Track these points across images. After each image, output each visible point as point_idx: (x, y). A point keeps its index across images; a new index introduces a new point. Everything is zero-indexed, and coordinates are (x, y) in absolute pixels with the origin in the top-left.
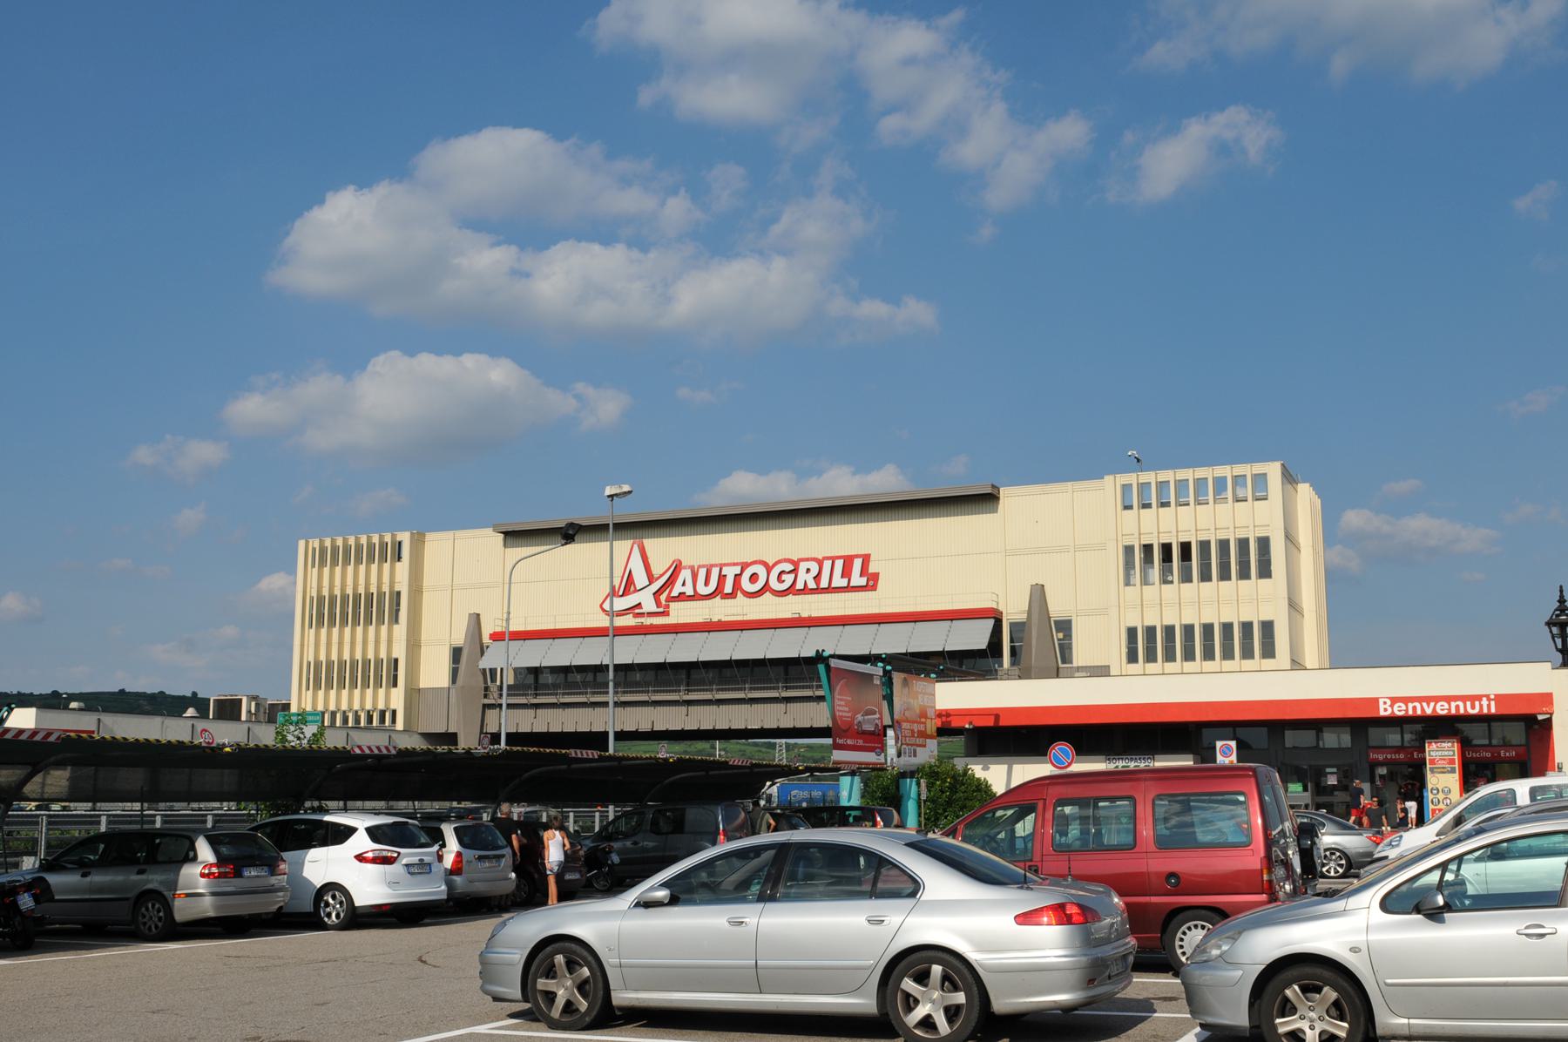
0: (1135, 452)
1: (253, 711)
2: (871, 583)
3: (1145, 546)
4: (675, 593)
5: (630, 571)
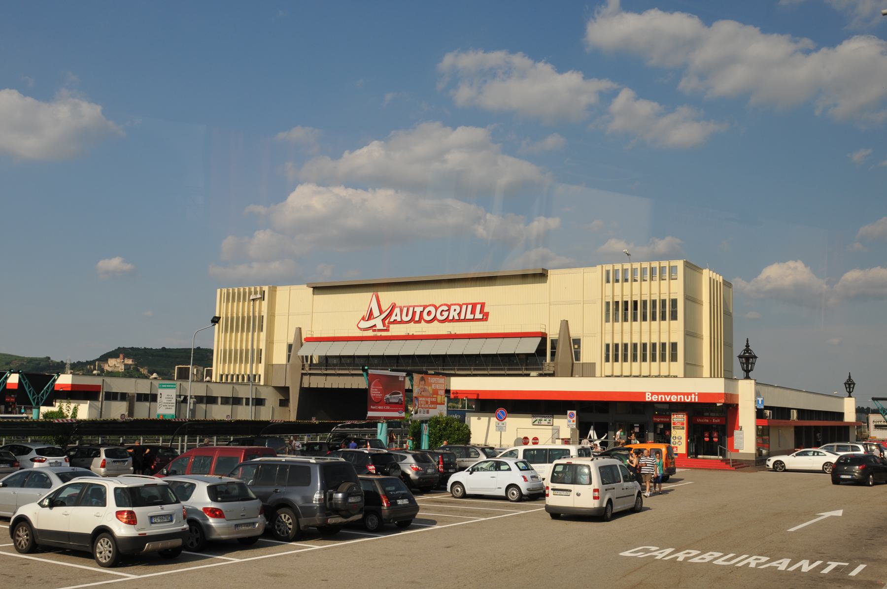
1: (195, 373)
2: (485, 317)
3: (616, 302)
4: (392, 320)
5: (371, 309)
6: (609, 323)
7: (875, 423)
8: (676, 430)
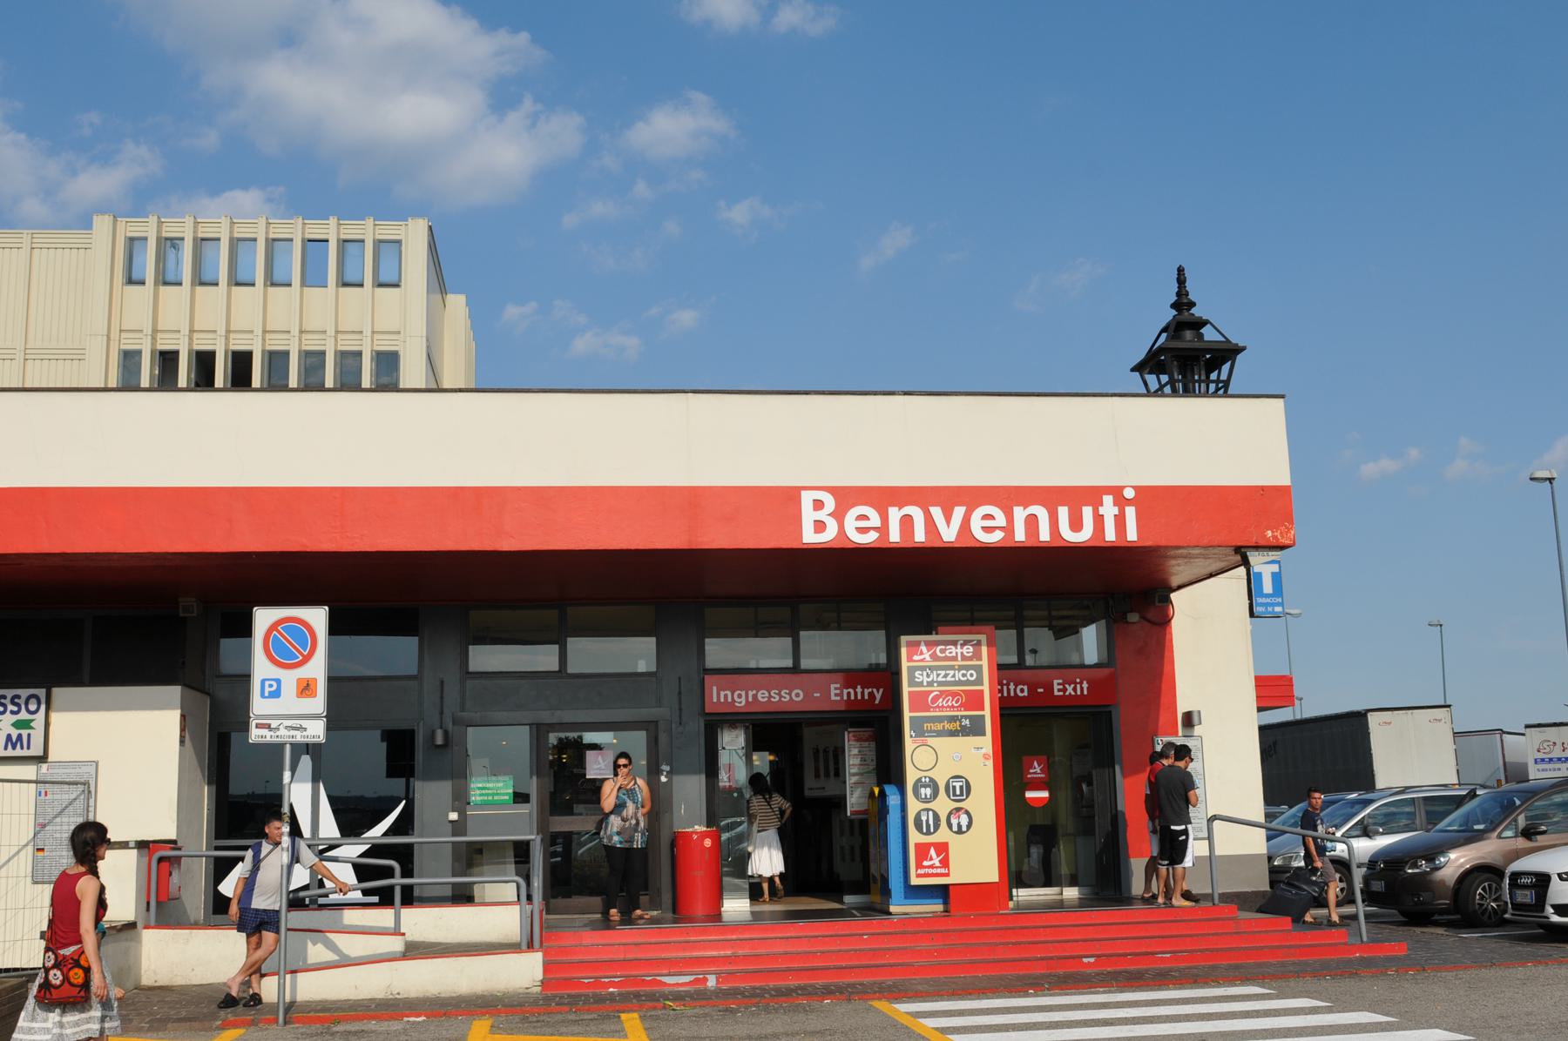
3: (163, 354)
8: (932, 741)
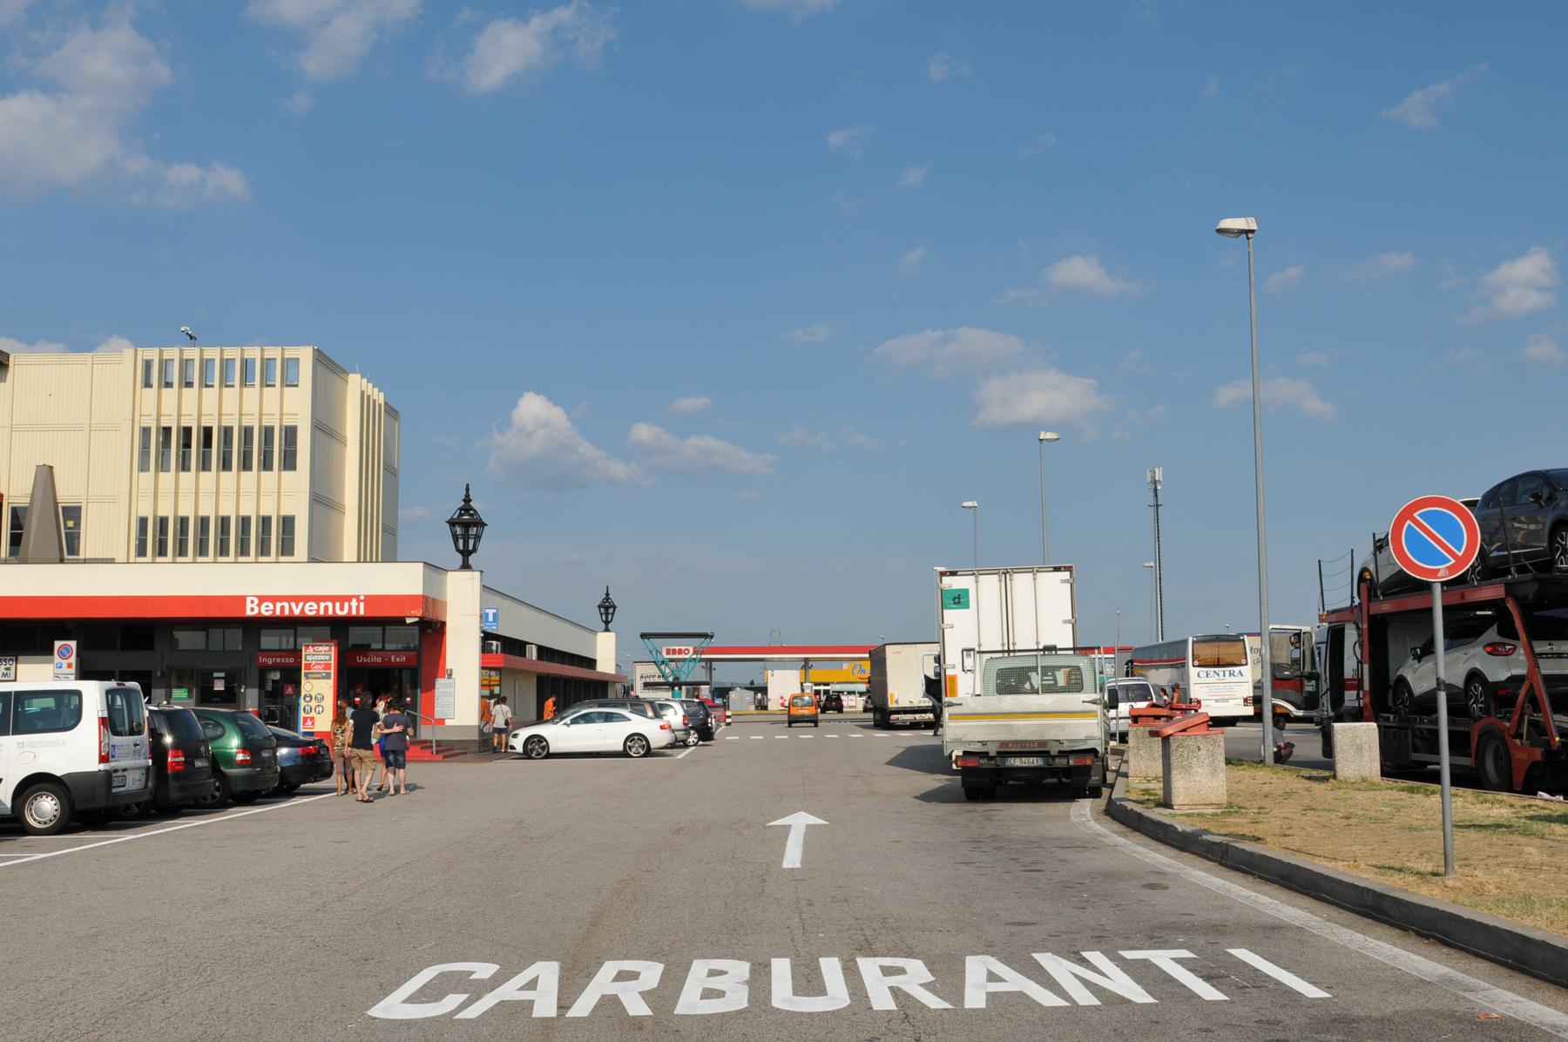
0: (188, 328)
6: (147, 473)
7: (644, 680)
8: (312, 681)
